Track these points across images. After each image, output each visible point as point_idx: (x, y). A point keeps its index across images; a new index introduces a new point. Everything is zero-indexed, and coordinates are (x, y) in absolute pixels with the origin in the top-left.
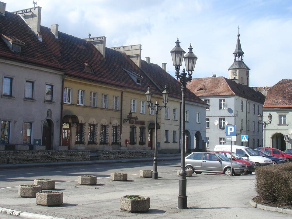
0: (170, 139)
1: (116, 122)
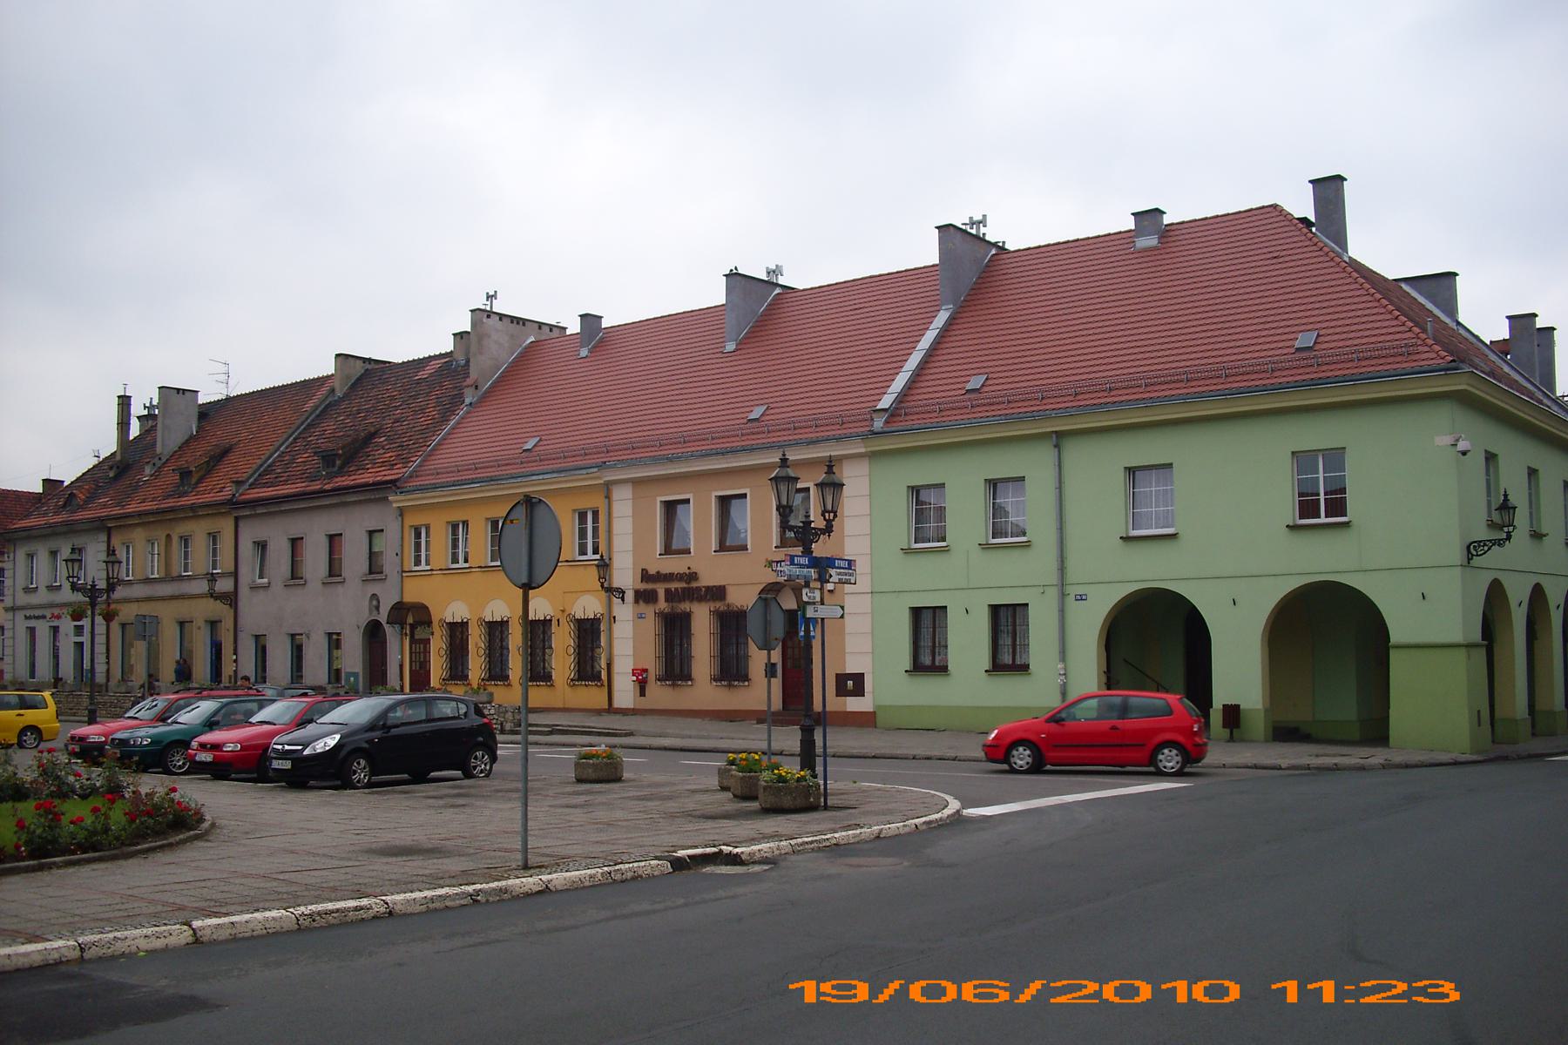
0: (476, 666)
1: (589, 606)
